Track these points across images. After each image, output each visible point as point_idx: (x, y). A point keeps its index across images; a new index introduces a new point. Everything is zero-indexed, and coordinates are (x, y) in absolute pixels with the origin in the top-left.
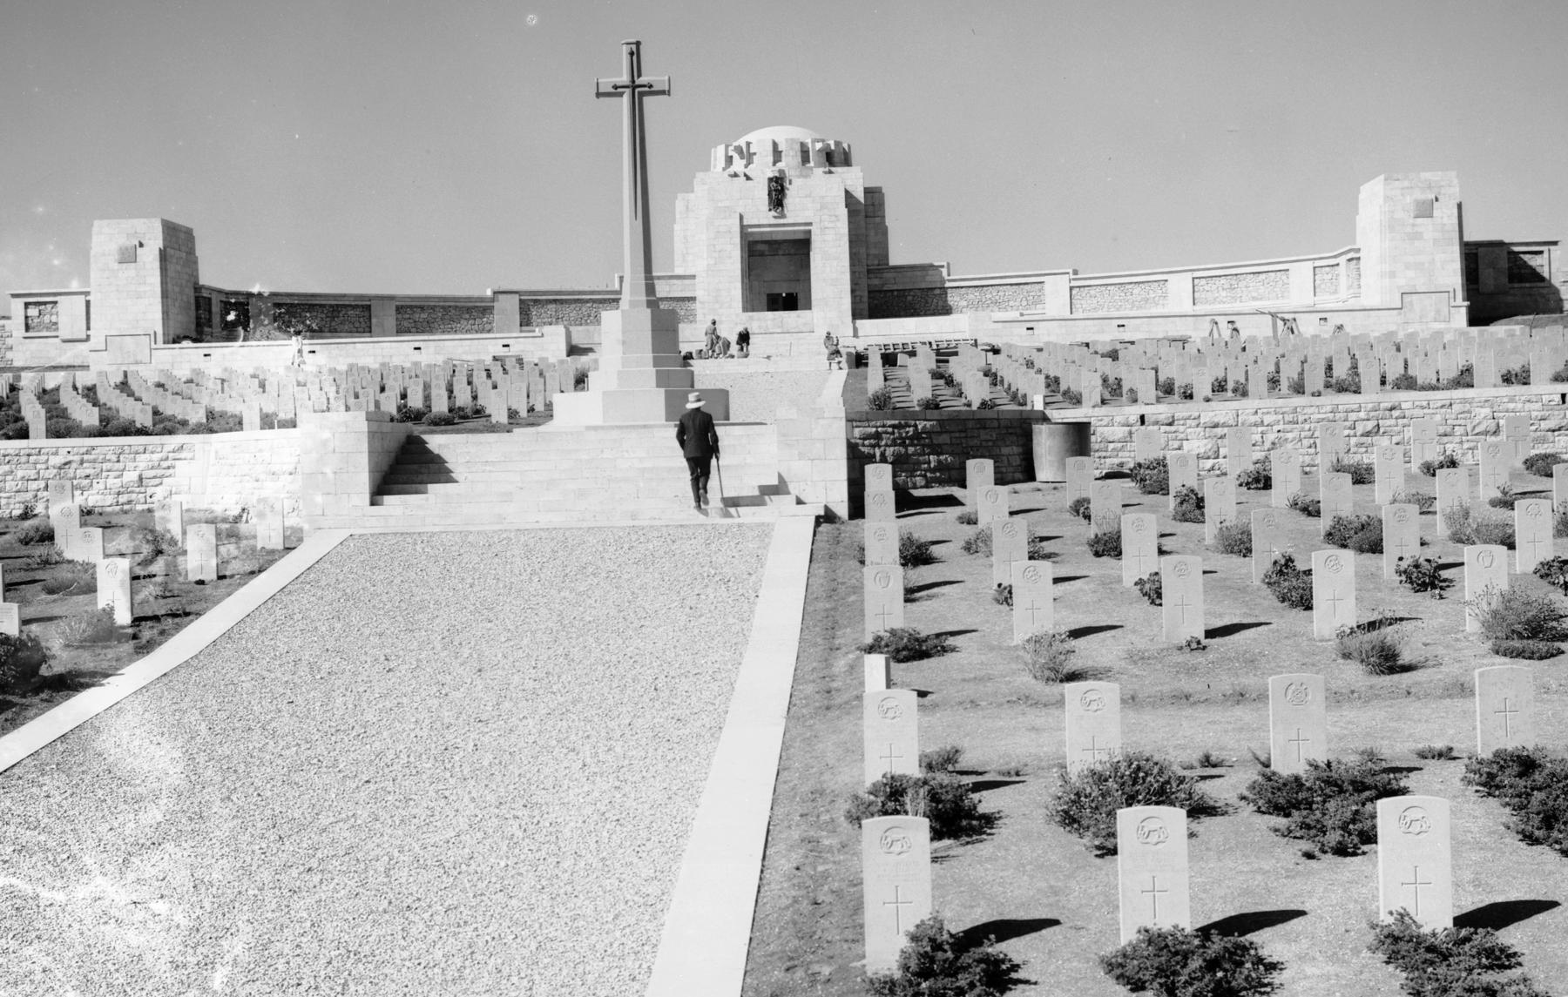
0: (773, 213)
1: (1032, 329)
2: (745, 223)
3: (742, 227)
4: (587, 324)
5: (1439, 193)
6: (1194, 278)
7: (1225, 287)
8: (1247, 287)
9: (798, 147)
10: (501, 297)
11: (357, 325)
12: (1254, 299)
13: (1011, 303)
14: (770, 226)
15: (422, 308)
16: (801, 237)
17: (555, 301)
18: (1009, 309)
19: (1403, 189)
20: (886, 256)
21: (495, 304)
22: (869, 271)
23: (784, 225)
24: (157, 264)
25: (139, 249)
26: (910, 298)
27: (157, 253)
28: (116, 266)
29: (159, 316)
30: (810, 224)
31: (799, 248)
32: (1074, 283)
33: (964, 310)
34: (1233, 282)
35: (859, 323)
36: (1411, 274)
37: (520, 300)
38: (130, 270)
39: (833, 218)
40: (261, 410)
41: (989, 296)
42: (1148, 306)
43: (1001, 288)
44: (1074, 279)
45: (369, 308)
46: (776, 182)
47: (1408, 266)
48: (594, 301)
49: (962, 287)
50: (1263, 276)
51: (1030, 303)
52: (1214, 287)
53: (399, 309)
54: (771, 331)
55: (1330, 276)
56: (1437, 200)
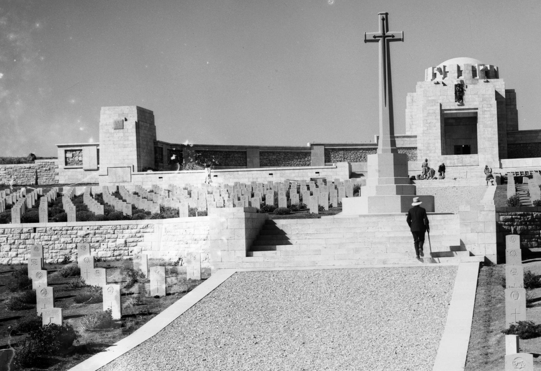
0: (457, 103)
1: (318, 173)
2: (443, 108)
3: (442, 111)
4: (360, 161)
9: (471, 68)
10: (315, 147)
11: (239, 162)
14: (456, 110)
15: (273, 153)
17: (343, 149)
22: (508, 134)
23: (463, 109)
24: (134, 130)
27: (134, 124)
28: (113, 131)
30: (477, 109)
37: (325, 149)
39: (489, 106)
46: (459, 87)
48: (363, 149)
53: (261, 154)
54: (457, 165)
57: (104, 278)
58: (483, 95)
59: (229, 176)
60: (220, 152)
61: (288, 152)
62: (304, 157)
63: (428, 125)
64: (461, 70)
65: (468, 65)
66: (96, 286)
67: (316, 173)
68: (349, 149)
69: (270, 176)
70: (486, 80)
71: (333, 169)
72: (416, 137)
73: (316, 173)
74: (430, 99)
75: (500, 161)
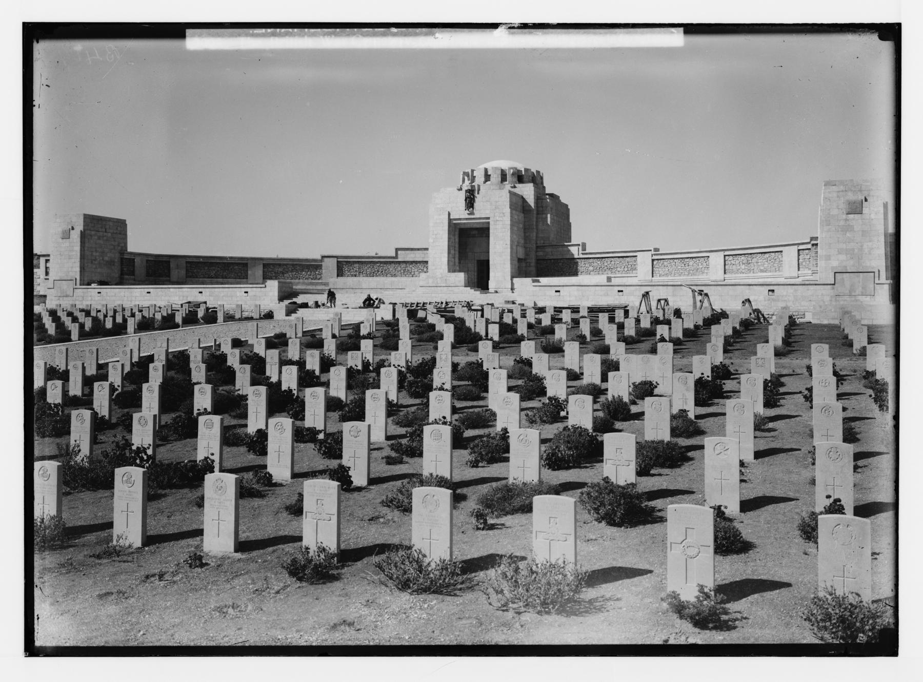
0: (467, 212)
1: (559, 291)
2: (451, 217)
3: (450, 220)
4: (377, 276)
5: (869, 195)
6: (725, 256)
7: (744, 262)
8: (757, 263)
9: (500, 172)
10: (326, 259)
11: (239, 274)
12: (762, 271)
13: (619, 269)
14: (467, 219)
15: (280, 265)
16: (485, 226)
17: (358, 262)
18: (617, 272)
19: (839, 192)
20: (126, 248)
21: (323, 263)
22: (537, 247)
23: (474, 219)
24: (79, 240)
25: (71, 231)
26: (560, 264)
27: (79, 233)
28: (60, 240)
29: (78, 269)
30: (488, 218)
31: (482, 232)
32: (655, 257)
33: (591, 273)
34: (749, 259)
35: (515, 280)
36: (842, 257)
37: (338, 261)
38: (66, 243)
39: (502, 215)
40: (360, 308)
41: (606, 264)
42: (697, 273)
43: (612, 259)
44: (655, 255)
45: (246, 265)
46: (469, 193)
47: (840, 253)
48: (381, 262)
49: (590, 258)
50: (767, 255)
51: (629, 269)
52: (737, 262)
53: (265, 266)
54: (439, 285)
55: (808, 257)
56: (866, 200)
57: (150, 430)
58: (496, 202)
59: (160, 293)
60: (217, 263)
61: (296, 264)
62: (315, 270)
63: (434, 236)
64: (489, 174)
65: (496, 168)
66: (431, 474)
67: (556, 291)
68: (365, 262)
69: (148, 294)
70: (513, 185)
71: (263, 289)
72: (427, 249)
73: (556, 291)
74: (438, 206)
75: (512, 280)
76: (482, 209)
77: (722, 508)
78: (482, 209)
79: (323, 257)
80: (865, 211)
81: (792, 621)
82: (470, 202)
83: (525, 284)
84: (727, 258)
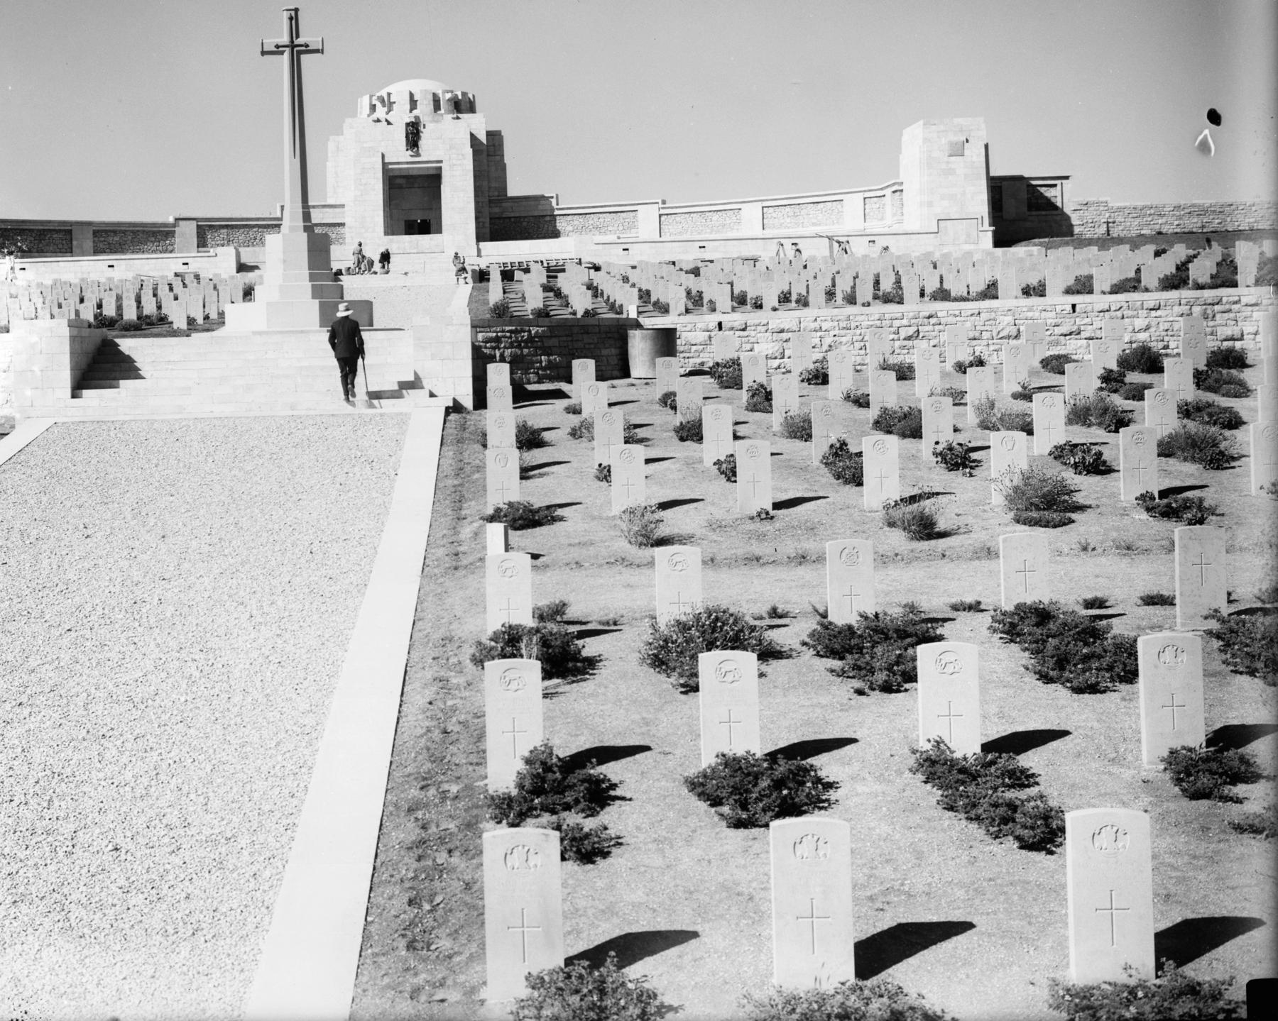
0: (410, 152)
2: (386, 161)
3: (384, 164)
4: (253, 246)
9: (431, 97)
11: (60, 246)
12: (814, 224)
13: (610, 228)
14: (408, 163)
15: (115, 232)
17: (227, 227)
22: (490, 201)
23: (419, 162)
30: (441, 162)
31: (431, 181)
32: (662, 212)
34: (797, 210)
35: (482, 244)
45: (70, 232)
48: (259, 226)
53: (96, 233)
56: (967, 141)
60: (30, 230)
75: (478, 245)
76: (431, 149)
77: (940, 448)
78: (431, 149)
79: (177, 220)
80: (967, 152)
81: (452, 826)
82: (413, 135)
83: (487, 246)
84: (765, 209)
